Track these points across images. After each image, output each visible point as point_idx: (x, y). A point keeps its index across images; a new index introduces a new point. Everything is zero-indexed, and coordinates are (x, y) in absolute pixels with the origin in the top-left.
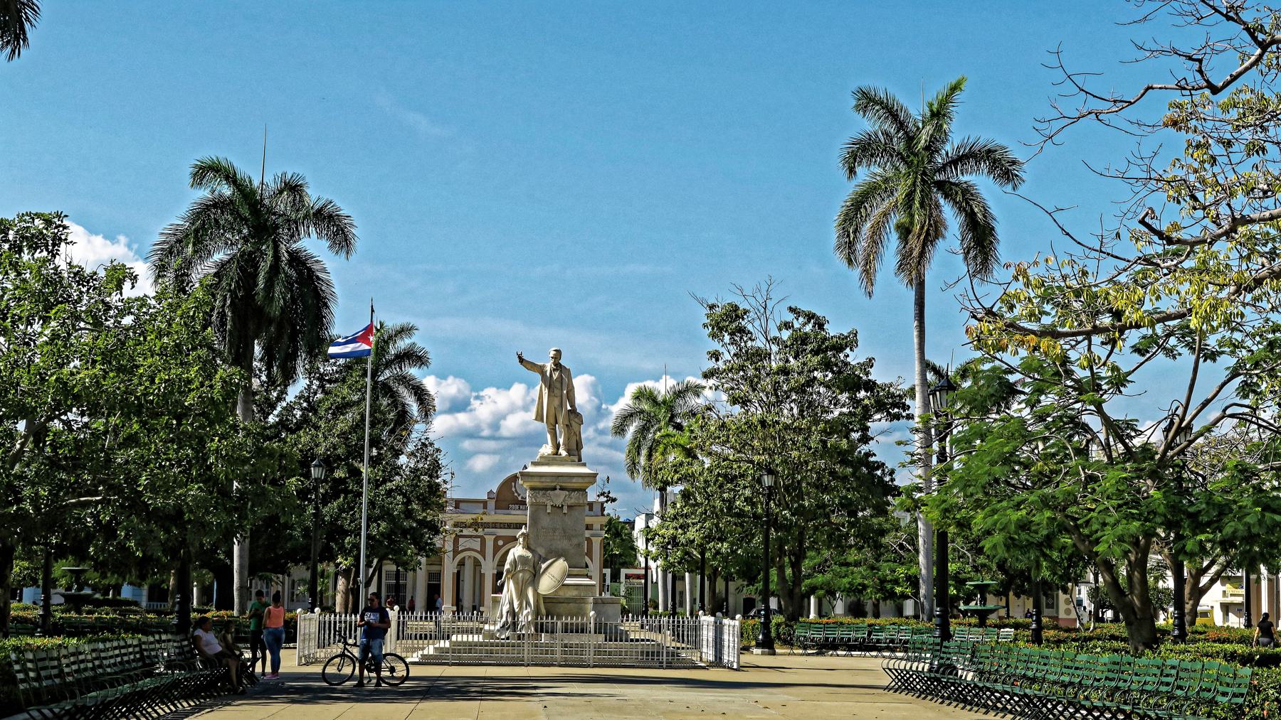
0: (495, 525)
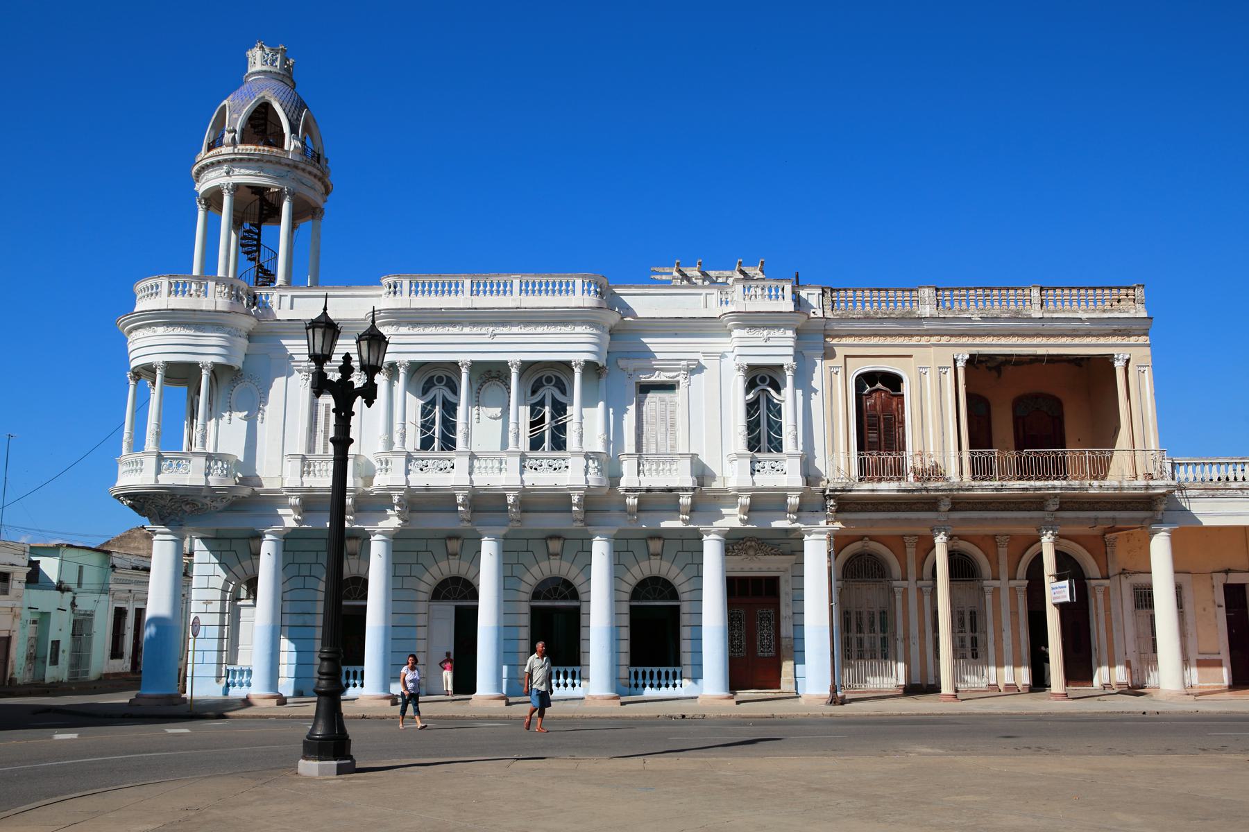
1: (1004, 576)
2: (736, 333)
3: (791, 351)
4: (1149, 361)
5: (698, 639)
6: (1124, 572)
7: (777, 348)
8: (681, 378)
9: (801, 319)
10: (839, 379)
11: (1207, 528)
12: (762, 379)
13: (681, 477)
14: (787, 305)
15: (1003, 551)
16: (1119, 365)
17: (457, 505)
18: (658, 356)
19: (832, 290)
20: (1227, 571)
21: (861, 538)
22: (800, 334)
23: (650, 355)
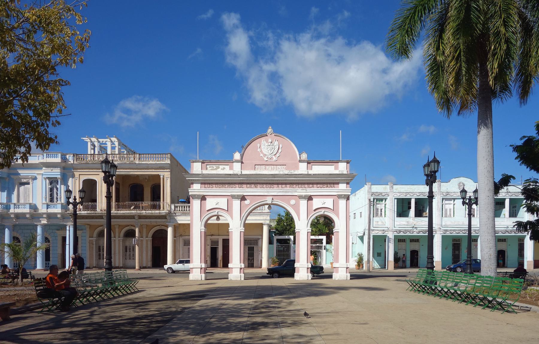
1: (144, 237)
2: (44, 168)
3: (59, 173)
4: (169, 176)
5: (244, 253)
6: (181, 235)
7: (56, 173)
8: (30, 181)
9: (64, 164)
10: (77, 182)
11: (180, 224)
12: (53, 181)
13: (27, 210)
14: (58, 160)
15: (145, 230)
16: (161, 177)
17: (531, 201)
18: (21, 175)
19: (77, 155)
20: (212, 235)
21: (129, 226)
22: (64, 168)
23: (19, 174)
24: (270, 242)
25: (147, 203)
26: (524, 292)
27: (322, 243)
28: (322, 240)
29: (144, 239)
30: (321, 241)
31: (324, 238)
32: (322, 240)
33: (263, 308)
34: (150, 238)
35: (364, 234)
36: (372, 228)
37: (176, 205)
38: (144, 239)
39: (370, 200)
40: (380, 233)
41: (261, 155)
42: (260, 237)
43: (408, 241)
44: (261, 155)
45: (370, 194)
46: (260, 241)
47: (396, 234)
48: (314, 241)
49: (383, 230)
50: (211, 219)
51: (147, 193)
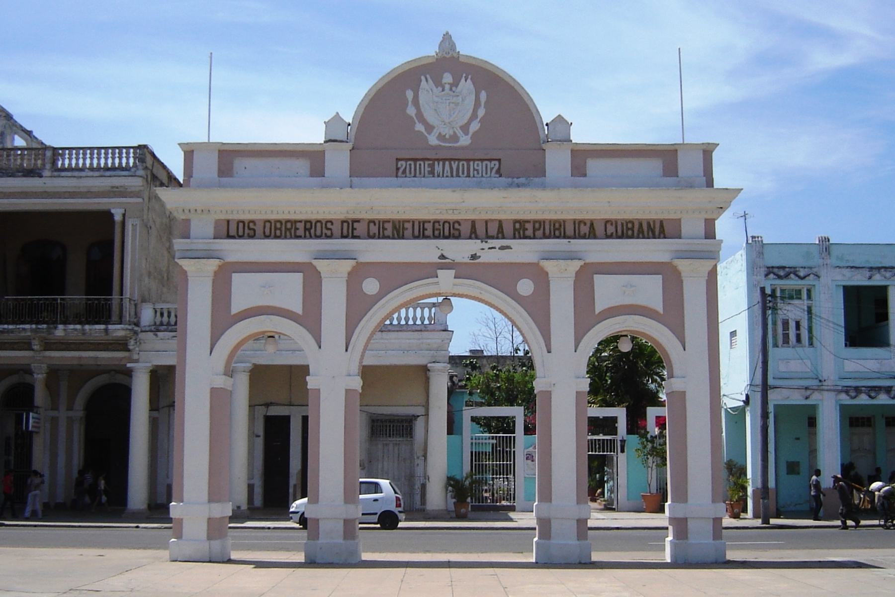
0: (587, 230)
24: (452, 427)
25: (76, 298)
26: (497, 393)
27: (614, 432)
28: (614, 420)
29: (62, 414)
30: (505, 425)
31: (620, 413)
32: (614, 420)
33: (428, 271)
34: (79, 412)
35: (747, 402)
36: (771, 381)
37: (159, 306)
38: (62, 414)
39: (763, 290)
40: (796, 398)
41: (419, 127)
42: (420, 411)
43: (880, 423)
44: (419, 127)
45: (763, 271)
46: (419, 425)
47: (845, 399)
48: (596, 425)
49: (807, 388)
50: (243, 348)
51: (76, 269)
